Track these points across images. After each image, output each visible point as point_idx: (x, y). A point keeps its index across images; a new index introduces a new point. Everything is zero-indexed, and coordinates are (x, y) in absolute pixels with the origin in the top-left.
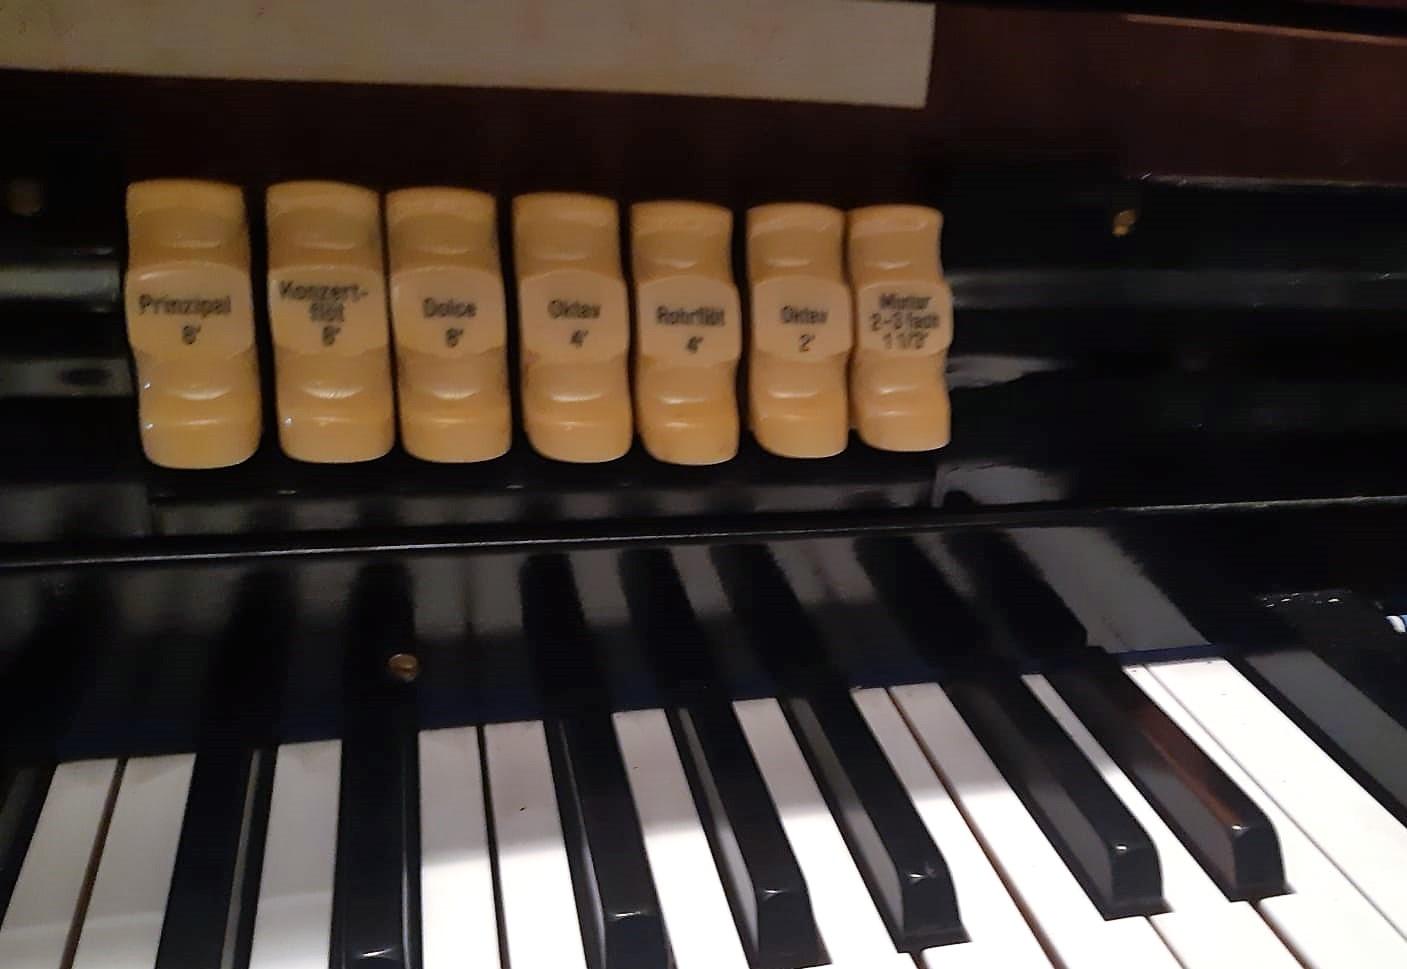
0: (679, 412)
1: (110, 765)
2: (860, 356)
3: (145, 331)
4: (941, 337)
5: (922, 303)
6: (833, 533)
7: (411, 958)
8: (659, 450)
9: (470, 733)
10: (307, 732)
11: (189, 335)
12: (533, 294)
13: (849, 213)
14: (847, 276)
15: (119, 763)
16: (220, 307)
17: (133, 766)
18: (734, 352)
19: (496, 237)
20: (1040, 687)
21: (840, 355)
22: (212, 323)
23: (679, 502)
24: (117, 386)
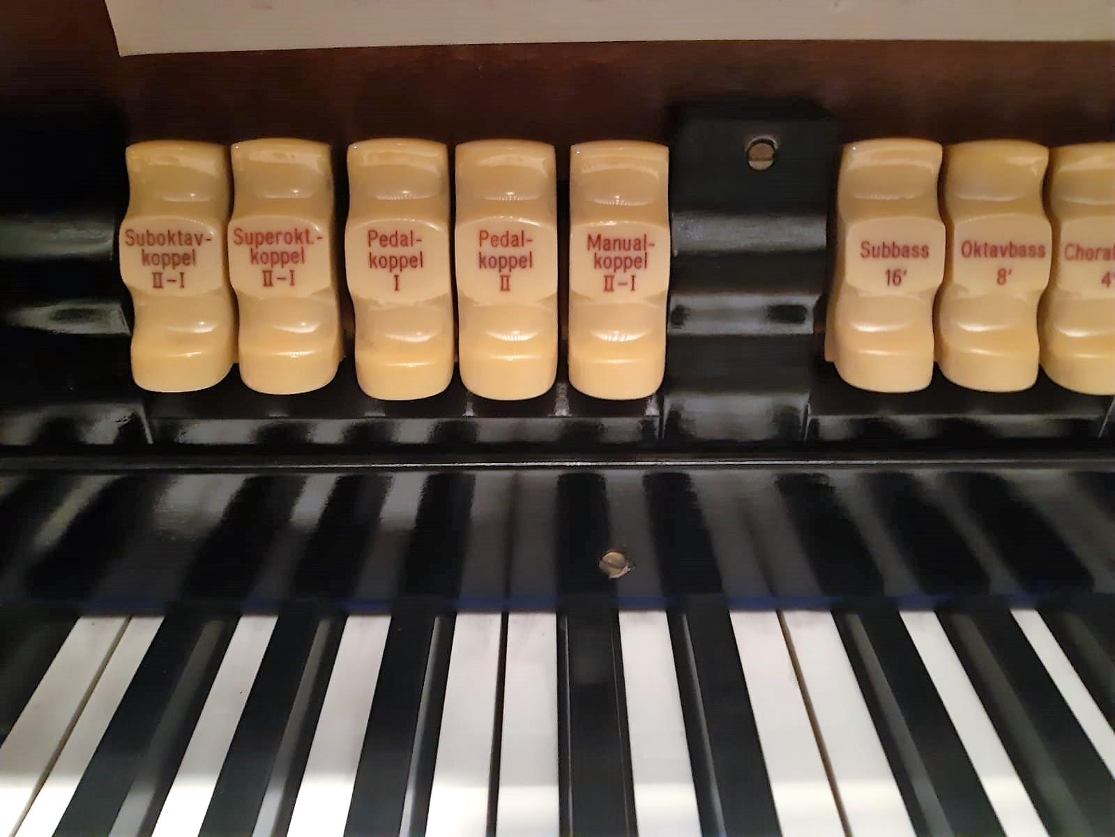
0: (302, 340)
1: (118, 622)
2: (1056, 298)
3: (133, 272)
4: (657, 275)
5: (517, 240)
6: (1014, 464)
7: (703, 751)
8: (958, 375)
9: (497, 619)
10: (369, 609)
11: (1002, 276)
12: (355, 233)
13: (949, 146)
14: (944, 213)
15: (125, 622)
16: (924, 252)
17: (134, 621)
18: (1043, 284)
19: (332, 182)
20: (1032, 625)
21: (1039, 291)
22: (911, 265)
23: (491, 429)
24: (114, 324)
